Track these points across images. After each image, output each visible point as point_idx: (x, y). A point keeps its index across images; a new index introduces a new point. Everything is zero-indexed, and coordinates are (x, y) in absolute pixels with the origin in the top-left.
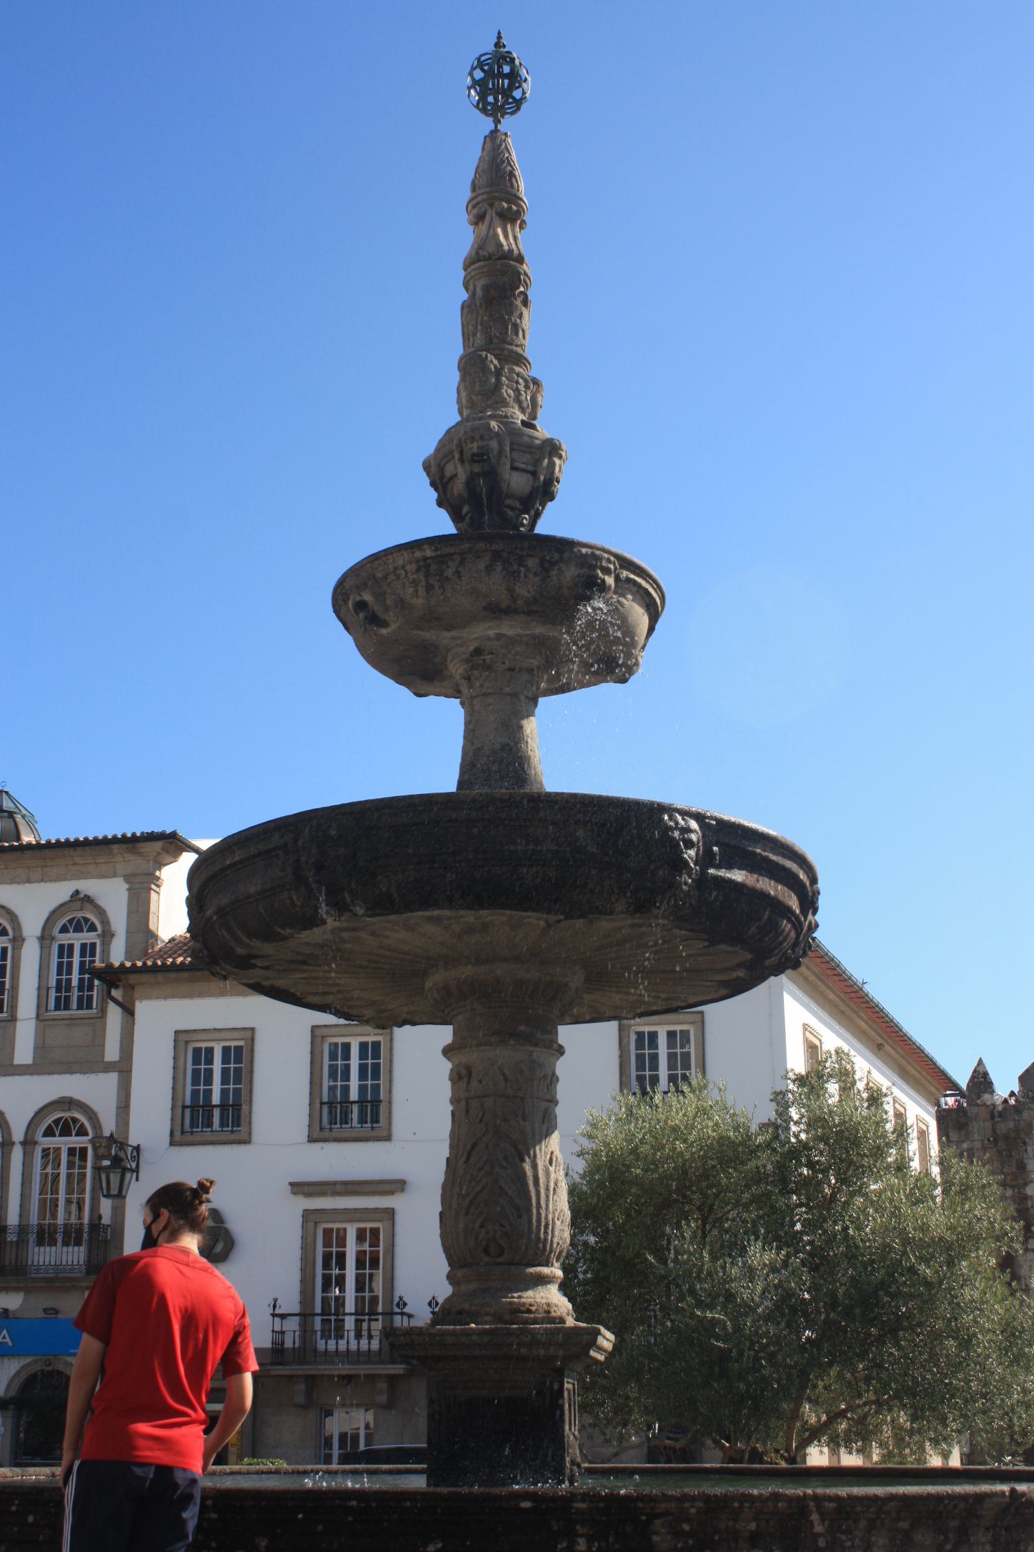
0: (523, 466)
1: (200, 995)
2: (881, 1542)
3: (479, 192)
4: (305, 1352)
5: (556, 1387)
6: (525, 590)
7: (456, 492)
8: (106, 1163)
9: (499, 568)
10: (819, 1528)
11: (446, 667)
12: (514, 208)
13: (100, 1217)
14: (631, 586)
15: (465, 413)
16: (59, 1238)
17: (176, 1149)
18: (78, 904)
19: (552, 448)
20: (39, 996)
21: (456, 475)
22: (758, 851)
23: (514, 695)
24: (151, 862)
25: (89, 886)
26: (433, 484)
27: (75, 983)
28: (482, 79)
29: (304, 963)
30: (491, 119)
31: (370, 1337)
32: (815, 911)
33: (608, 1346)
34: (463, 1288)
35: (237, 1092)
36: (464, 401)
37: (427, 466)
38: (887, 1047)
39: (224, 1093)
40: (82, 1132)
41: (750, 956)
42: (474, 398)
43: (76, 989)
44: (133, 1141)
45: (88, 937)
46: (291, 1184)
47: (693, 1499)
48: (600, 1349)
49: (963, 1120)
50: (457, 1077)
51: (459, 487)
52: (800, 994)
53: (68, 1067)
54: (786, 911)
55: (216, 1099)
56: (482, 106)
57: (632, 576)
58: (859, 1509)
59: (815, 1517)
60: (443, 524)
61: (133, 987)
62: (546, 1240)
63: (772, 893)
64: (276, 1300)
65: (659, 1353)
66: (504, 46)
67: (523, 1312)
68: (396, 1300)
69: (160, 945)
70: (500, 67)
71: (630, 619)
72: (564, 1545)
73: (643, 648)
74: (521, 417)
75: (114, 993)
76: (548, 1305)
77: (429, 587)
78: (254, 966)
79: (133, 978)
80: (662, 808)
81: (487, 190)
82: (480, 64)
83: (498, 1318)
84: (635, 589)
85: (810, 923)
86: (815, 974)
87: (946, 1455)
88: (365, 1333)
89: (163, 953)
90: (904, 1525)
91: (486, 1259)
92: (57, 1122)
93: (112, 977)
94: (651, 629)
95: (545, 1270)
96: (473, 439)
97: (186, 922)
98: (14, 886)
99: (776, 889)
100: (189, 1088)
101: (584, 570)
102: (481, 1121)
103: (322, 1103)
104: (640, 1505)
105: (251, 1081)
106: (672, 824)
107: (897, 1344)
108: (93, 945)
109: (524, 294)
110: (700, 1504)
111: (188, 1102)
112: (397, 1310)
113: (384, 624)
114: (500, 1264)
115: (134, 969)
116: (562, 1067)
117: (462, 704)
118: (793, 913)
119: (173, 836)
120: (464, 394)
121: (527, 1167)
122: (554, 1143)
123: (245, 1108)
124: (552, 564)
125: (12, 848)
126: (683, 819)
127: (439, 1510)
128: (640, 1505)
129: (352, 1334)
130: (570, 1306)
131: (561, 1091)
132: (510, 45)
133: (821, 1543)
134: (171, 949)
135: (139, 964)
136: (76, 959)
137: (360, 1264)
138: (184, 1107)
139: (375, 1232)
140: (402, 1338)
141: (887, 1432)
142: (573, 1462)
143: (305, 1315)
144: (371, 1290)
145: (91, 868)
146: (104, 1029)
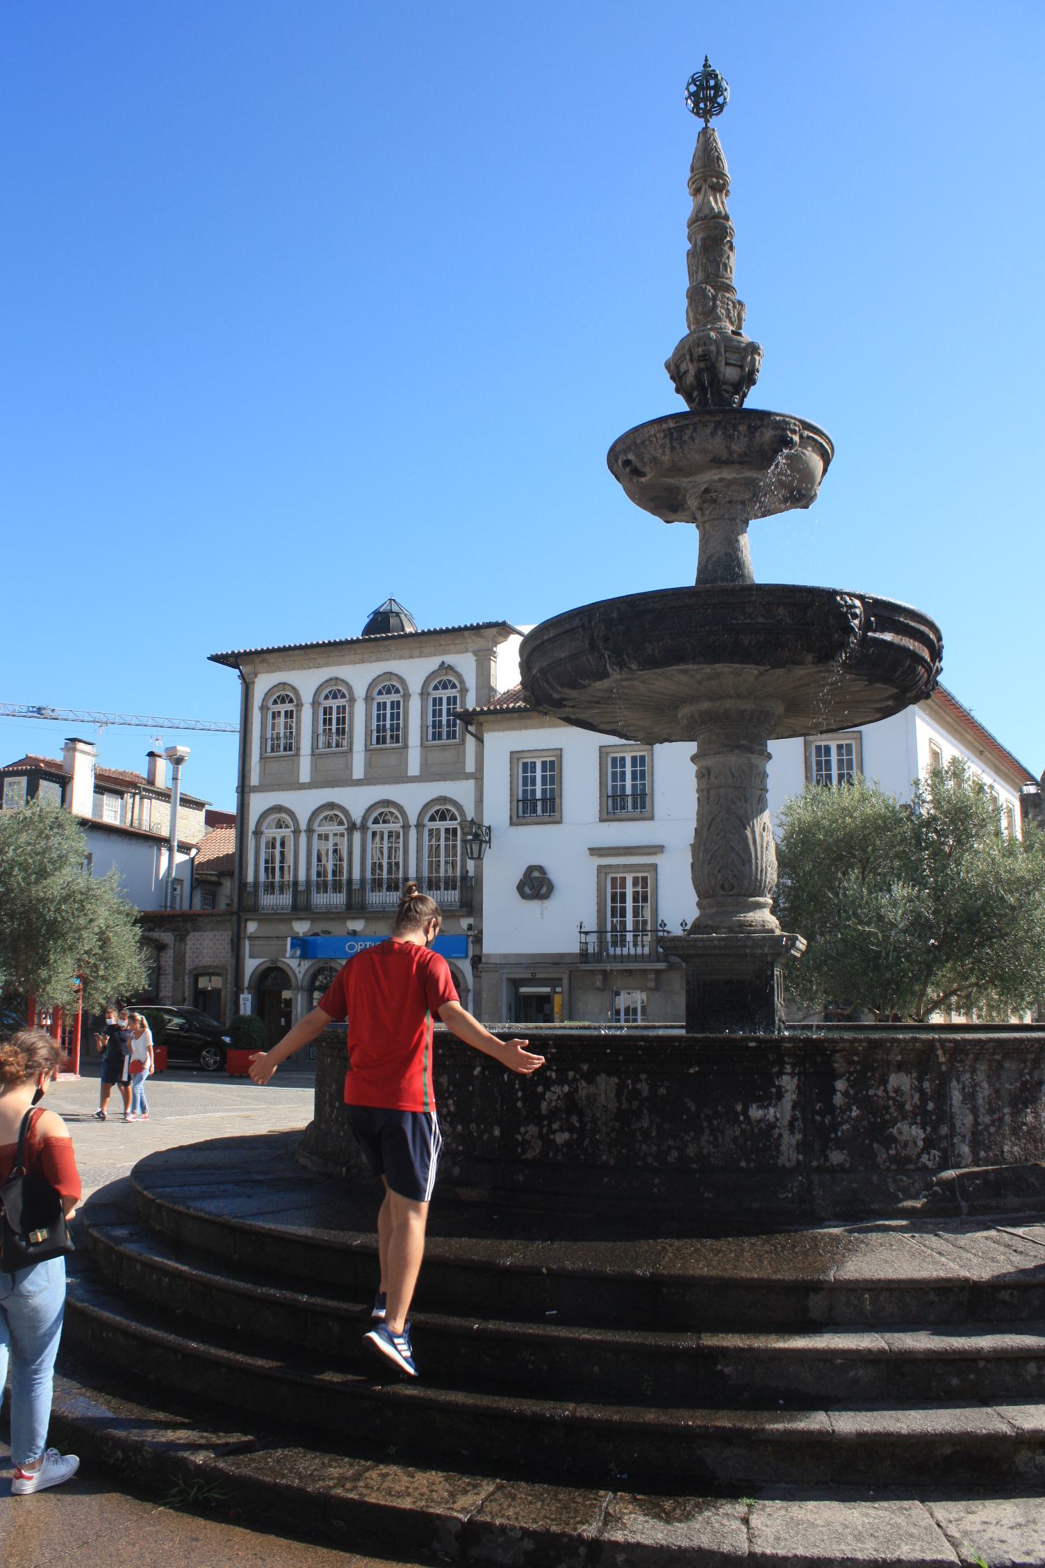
0: (733, 362)
1: (526, 728)
2: (983, 1068)
3: (696, 172)
4: (599, 957)
5: (769, 973)
6: (738, 447)
7: (688, 382)
8: (470, 837)
9: (720, 433)
10: (942, 1059)
11: (686, 503)
12: (721, 182)
13: (467, 872)
14: (811, 441)
15: (693, 327)
16: (442, 885)
17: (514, 828)
18: (445, 671)
19: (753, 349)
20: (422, 732)
21: (688, 371)
22: (902, 619)
23: (734, 519)
24: (490, 642)
25: (450, 659)
26: (672, 378)
27: (444, 722)
28: (695, 92)
29: (598, 702)
30: (702, 120)
31: (643, 946)
32: (940, 660)
33: (803, 947)
34: (708, 911)
35: (552, 790)
36: (692, 320)
37: (668, 366)
38: (986, 753)
39: (544, 791)
40: (453, 818)
41: (895, 690)
42: (698, 316)
43: (445, 727)
44: (486, 823)
45: (451, 692)
46: (590, 849)
47: (861, 1041)
48: (798, 949)
49: (1037, 801)
50: (701, 776)
51: (690, 379)
52: (927, 718)
53: (442, 777)
54: (921, 660)
55: (539, 795)
56: (697, 111)
57: (811, 435)
58: (968, 1047)
59: (940, 1052)
60: (681, 405)
61: (481, 724)
62: (761, 879)
63: (911, 648)
64: (581, 923)
65: (833, 954)
66: (710, 66)
67: (747, 926)
68: (660, 922)
69: (498, 696)
70: (708, 82)
71: (810, 464)
72: (777, 1069)
73: (820, 484)
74: (731, 328)
75: (470, 728)
76: (763, 921)
77: (673, 449)
78: (565, 706)
79: (482, 718)
80: (834, 593)
81: (702, 170)
82: (694, 81)
83: (730, 930)
84: (813, 443)
85: (937, 668)
86: (937, 704)
87: (1021, 1018)
88: (640, 943)
89: (500, 701)
90: (998, 1057)
91: (723, 892)
92: (437, 812)
93: (468, 718)
94: (825, 471)
95: (761, 899)
96: (699, 345)
97: (518, 678)
98: (403, 661)
99: (914, 645)
100: (521, 788)
101: (779, 431)
102: (717, 804)
103: (608, 797)
104: (826, 1044)
105: (561, 783)
106: (842, 602)
107: (991, 947)
108: (455, 698)
109: (730, 242)
110: (865, 1044)
111: (521, 798)
112: (660, 928)
113: (643, 474)
114: (731, 896)
115: (482, 712)
116: (770, 767)
117: (697, 527)
118: (925, 661)
119: (504, 624)
120: (691, 315)
121: (748, 833)
122: (766, 817)
123: (557, 800)
124: (757, 428)
125: (400, 637)
126: (851, 599)
127: (697, 1048)
128: (826, 1044)
129: (631, 944)
130: (778, 922)
131: (770, 783)
132: (715, 65)
133: (944, 1068)
134: (505, 698)
135: (485, 709)
136: (444, 707)
137: (635, 900)
138: (518, 801)
139: (645, 879)
140: (668, 943)
141: (983, 1002)
142: (780, 1020)
143: (601, 932)
144: (643, 917)
145: (451, 647)
146: (464, 752)
